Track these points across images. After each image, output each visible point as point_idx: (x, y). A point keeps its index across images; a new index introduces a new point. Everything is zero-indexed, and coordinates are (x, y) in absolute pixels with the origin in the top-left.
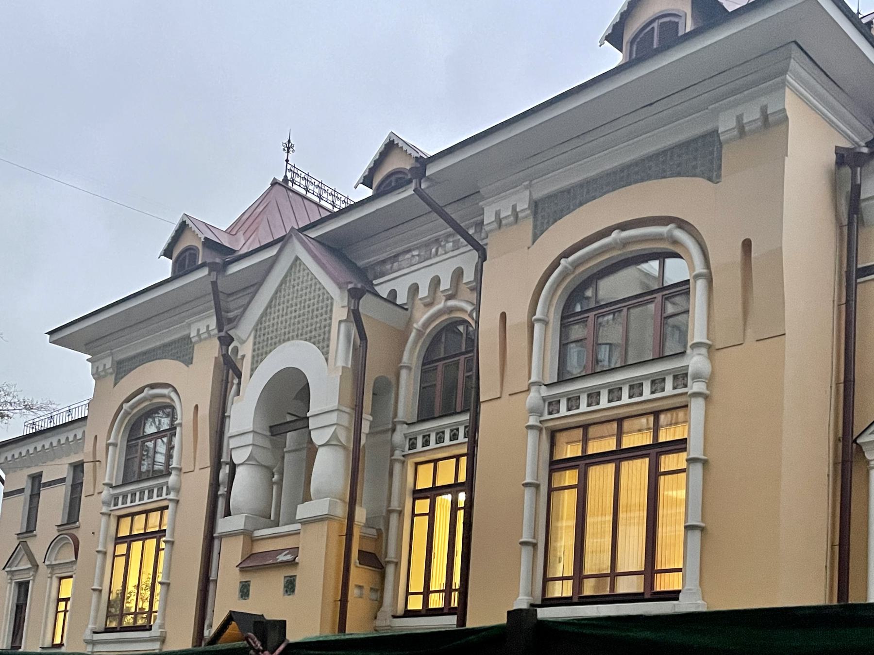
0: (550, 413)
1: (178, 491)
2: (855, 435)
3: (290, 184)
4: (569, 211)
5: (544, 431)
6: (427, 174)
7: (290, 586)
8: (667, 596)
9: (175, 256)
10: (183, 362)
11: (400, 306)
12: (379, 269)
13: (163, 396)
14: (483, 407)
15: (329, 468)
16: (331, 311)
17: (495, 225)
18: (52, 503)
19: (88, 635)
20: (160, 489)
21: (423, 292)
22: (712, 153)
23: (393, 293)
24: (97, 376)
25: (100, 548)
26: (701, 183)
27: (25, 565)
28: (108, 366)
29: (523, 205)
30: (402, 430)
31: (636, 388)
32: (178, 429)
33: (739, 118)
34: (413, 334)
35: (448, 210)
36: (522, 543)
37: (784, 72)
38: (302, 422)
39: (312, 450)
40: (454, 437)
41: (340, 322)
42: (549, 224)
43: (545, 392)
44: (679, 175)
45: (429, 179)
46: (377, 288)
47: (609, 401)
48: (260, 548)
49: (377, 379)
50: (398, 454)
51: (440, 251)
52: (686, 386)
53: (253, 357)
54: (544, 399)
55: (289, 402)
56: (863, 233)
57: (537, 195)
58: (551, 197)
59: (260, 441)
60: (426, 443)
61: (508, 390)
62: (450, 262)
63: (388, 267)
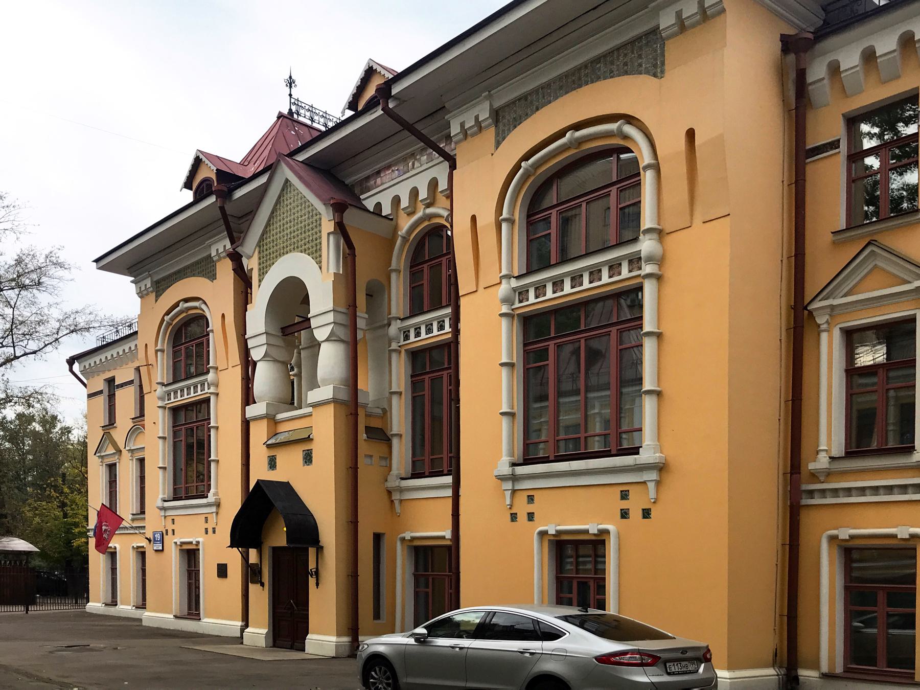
0: (521, 302)
1: (217, 386)
2: (806, 303)
3: (295, 116)
4: (527, 116)
5: (516, 318)
6: (394, 92)
7: (308, 458)
8: (632, 451)
9: (194, 188)
10: (208, 278)
11: (385, 217)
12: (364, 185)
13: (196, 308)
15: (330, 360)
16: (320, 225)
17: (461, 136)
18: (126, 400)
20: (203, 385)
21: (405, 203)
22: (656, 51)
23: (378, 205)
24: (141, 294)
26: (646, 81)
27: (111, 450)
28: (149, 285)
29: (484, 115)
32: (211, 334)
33: (679, 14)
35: (419, 127)
36: (502, 414)
39: (315, 345)
40: (441, 327)
41: (329, 234)
42: (510, 131)
43: (514, 283)
45: (395, 98)
46: (364, 202)
47: (572, 287)
49: (369, 283)
50: (394, 346)
51: (417, 164)
52: (640, 269)
53: (260, 269)
54: (514, 290)
56: (811, 117)
57: (497, 105)
59: (273, 341)
60: (418, 334)
61: (482, 284)
62: (424, 173)
63: (372, 182)
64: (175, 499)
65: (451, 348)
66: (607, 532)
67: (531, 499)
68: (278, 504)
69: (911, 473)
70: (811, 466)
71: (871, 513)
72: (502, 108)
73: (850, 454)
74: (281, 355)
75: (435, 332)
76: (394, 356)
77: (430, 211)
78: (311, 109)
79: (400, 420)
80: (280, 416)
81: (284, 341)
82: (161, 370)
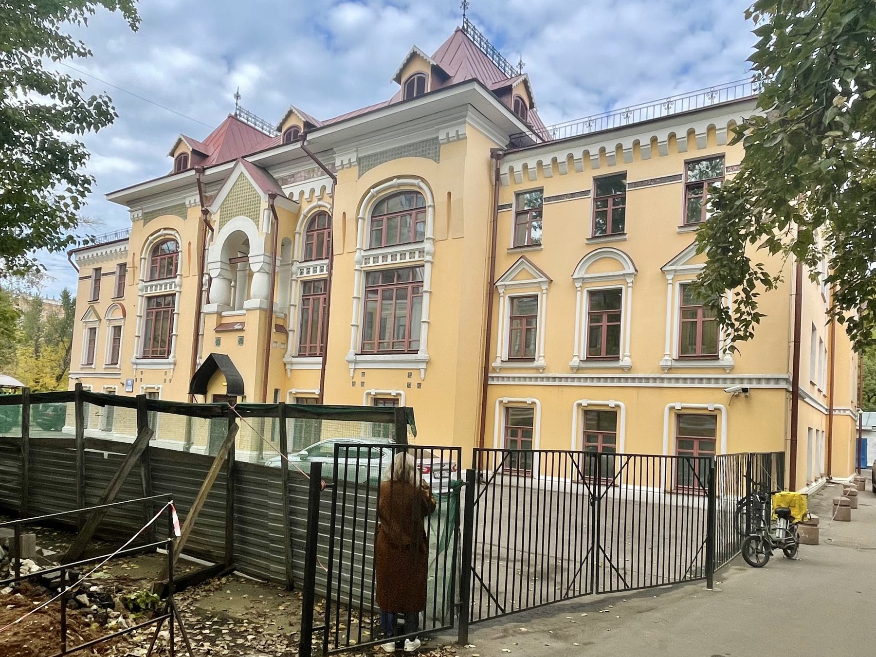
1: (181, 286)
6: (308, 138)
7: (241, 341)
14: (335, 257)
15: (259, 283)
18: (108, 285)
19: (134, 360)
20: (171, 284)
23: (291, 194)
25: (355, 295)
29: (353, 160)
30: (296, 265)
31: (403, 255)
34: (302, 216)
35: (316, 156)
37: (465, 116)
38: (245, 257)
39: (251, 275)
40: (322, 270)
43: (363, 253)
44: (422, 156)
48: (225, 321)
50: (294, 277)
55: (238, 247)
57: (360, 156)
58: (368, 157)
59: (225, 267)
60: (308, 272)
61: (346, 251)
64: (144, 358)
65: (326, 283)
66: (400, 395)
67: (363, 374)
68: (222, 369)
69: (533, 371)
70: (493, 364)
71: (517, 390)
72: (363, 157)
73: (681, 358)
74: (229, 275)
75: (318, 273)
76: (294, 283)
77: (320, 203)
78: (248, 113)
79: (294, 322)
80: (224, 314)
81: (231, 267)
82: (143, 270)
